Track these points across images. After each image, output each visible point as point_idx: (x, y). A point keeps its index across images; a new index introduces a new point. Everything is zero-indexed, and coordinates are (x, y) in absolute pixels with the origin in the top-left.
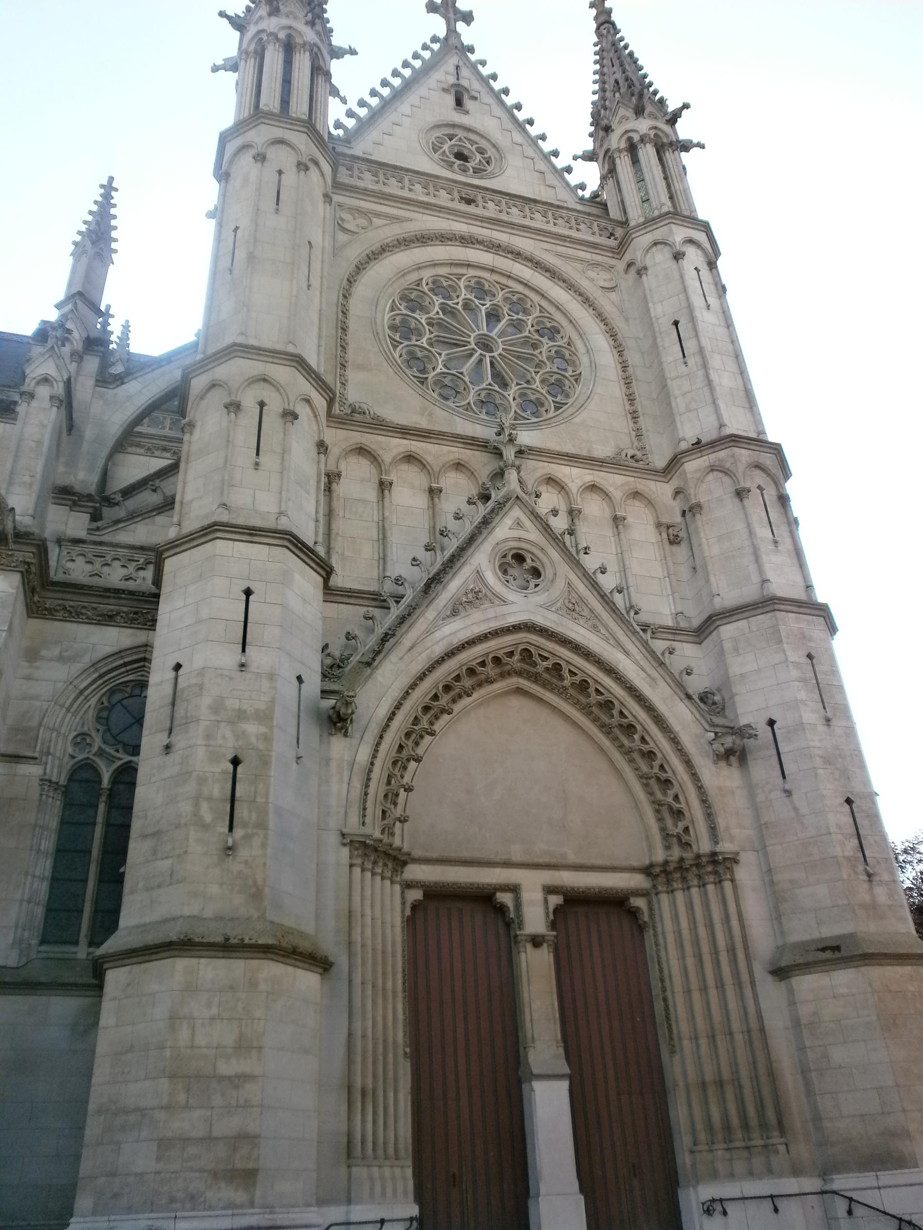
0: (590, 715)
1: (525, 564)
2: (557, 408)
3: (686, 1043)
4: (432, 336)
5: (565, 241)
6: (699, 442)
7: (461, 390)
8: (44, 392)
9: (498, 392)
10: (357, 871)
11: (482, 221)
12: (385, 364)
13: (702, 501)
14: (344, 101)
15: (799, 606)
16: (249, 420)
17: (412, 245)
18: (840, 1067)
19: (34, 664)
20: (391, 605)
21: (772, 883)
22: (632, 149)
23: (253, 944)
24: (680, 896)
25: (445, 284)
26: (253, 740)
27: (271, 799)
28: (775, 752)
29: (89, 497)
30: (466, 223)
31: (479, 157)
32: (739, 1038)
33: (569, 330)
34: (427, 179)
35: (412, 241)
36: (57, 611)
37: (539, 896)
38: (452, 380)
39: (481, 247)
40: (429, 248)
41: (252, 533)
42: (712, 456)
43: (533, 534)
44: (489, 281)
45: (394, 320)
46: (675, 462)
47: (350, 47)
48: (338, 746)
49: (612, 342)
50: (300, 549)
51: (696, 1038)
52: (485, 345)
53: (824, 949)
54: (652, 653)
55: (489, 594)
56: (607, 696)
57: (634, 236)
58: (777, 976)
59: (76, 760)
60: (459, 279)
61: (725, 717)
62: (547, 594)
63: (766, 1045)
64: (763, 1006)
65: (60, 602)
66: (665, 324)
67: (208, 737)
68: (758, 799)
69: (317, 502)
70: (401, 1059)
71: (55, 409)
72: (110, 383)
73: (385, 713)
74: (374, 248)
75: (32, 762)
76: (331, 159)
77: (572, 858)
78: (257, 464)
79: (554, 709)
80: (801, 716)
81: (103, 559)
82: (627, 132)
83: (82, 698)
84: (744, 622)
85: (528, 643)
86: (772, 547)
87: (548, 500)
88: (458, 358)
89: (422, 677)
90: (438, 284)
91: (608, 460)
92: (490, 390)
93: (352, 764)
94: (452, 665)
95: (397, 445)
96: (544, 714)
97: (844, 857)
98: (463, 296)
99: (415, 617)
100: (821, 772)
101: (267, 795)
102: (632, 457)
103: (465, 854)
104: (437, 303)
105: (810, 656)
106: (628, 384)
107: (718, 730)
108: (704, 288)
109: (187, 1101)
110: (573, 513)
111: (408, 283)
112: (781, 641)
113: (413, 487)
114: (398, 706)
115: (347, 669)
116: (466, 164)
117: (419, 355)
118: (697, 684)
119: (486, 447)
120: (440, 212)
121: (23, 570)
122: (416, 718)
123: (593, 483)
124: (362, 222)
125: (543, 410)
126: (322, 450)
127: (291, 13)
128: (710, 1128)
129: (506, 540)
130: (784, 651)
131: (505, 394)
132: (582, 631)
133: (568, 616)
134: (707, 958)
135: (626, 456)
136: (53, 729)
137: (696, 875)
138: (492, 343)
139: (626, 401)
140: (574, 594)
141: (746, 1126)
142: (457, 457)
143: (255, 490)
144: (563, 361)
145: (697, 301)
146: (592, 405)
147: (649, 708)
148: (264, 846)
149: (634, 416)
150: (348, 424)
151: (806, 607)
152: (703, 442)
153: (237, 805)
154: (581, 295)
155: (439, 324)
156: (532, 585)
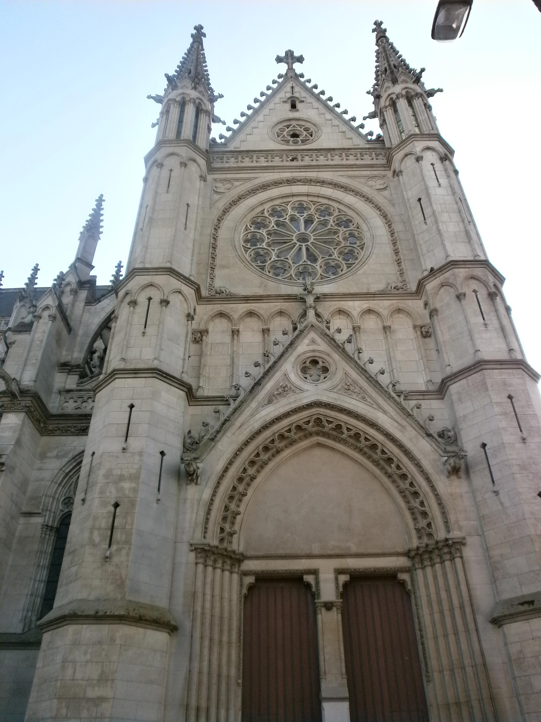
1: (318, 366)
2: (348, 267)
3: (436, 676)
4: (269, 240)
5: (353, 168)
6: (432, 269)
7: (287, 268)
8: (46, 314)
9: (310, 265)
10: (201, 567)
11: (299, 169)
12: (239, 262)
14: (224, 123)
15: (501, 364)
16: (141, 310)
17: (258, 192)
19: (44, 461)
20: (231, 403)
21: (490, 558)
22: (393, 104)
23: (112, 615)
24: (429, 570)
25: (279, 209)
26: (127, 492)
27: (134, 526)
28: (486, 465)
29: (78, 366)
30: (332, 171)
31: (305, 133)
32: (469, 670)
33: (357, 219)
34: (280, 153)
36: (55, 430)
37: (332, 576)
38: (282, 264)
39: (301, 183)
40: (268, 191)
41: (136, 372)
43: (322, 346)
44: (306, 202)
45: (247, 236)
46: (421, 285)
47: (219, 94)
48: (192, 491)
50: (165, 377)
51: (441, 671)
52: (303, 239)
53: (522, 604)
54: (403, 409)
55: (292, 387)
56: (373, 441)
58: (496, 624)
59: (64, 512)
60: (287, 205)
61: (457, 446)
62: (331, 381)
63: (488, 677)
64: (485, 646)
65: (56, 425)
66: (414, 201)
67: (101, 492)
68: (478, 500)
69: (185, 348)
70: (233, 687)
71: (51, 322)
72: (93, 303)
74: (233, 199)
75: (38, 515)
76: (204, 156)
77: (354, 549)
78: (144, 333)
79: (343, 454)
80: (502, 439)
81: (82, 399)
82: (389, 95)
83: (68, 477)
84: (464, 381)
86: (483, 328)
87: (338, 322)
88: (286, 250)
89: (246, 443)
90: (275, 210)
91: (378, 293)
92: (305, 265)
93: (199, 501)
94: (268, 433)
95: (243, 307)
98: (289, 214)
99: (243, 408)
100: (518, 476)
101: (132, 524)
102: (395, 288)
103: (281, 552)
104: (273, 221)
105: (510, 397)
106: (394, 244)
107: (449, 454)
109: (67, 715)
110: (356, 329)
111: (256, 213)
112: (487, 389)
114: (231, 463)
115: (201, 444)
117: (262, 253)
118: (435, 427)
119: (296, 299)
120: (274, 169)
121: (25, 410)
122: (245, 469)
123: (368, 308)
124: (228, 186)
125: (339, 270)
126: (189, 318)
127: (184, 86)
129: (305, 353)
130: (489, 396)
131: (314, 265)
132: (354, 402)
133: (345, 394)
134: (447, 613)
135: (391, 288)
136: (50, 497)
137: (438, 555)
138: (307, 236)
140: (350, 380)
142: (279, 307)
143: (142, 348)
144: (355, 238)
145: (432, 183)
146: (371, 261)
147: (401, 446)
148: (128, 555)
149: (399, 263)
150: (263, 299)
151: (506, 364)
152: (435, 268)
153: (114, 531)
154: (363, 197)
155: (275, 233)
156: (322, 377)
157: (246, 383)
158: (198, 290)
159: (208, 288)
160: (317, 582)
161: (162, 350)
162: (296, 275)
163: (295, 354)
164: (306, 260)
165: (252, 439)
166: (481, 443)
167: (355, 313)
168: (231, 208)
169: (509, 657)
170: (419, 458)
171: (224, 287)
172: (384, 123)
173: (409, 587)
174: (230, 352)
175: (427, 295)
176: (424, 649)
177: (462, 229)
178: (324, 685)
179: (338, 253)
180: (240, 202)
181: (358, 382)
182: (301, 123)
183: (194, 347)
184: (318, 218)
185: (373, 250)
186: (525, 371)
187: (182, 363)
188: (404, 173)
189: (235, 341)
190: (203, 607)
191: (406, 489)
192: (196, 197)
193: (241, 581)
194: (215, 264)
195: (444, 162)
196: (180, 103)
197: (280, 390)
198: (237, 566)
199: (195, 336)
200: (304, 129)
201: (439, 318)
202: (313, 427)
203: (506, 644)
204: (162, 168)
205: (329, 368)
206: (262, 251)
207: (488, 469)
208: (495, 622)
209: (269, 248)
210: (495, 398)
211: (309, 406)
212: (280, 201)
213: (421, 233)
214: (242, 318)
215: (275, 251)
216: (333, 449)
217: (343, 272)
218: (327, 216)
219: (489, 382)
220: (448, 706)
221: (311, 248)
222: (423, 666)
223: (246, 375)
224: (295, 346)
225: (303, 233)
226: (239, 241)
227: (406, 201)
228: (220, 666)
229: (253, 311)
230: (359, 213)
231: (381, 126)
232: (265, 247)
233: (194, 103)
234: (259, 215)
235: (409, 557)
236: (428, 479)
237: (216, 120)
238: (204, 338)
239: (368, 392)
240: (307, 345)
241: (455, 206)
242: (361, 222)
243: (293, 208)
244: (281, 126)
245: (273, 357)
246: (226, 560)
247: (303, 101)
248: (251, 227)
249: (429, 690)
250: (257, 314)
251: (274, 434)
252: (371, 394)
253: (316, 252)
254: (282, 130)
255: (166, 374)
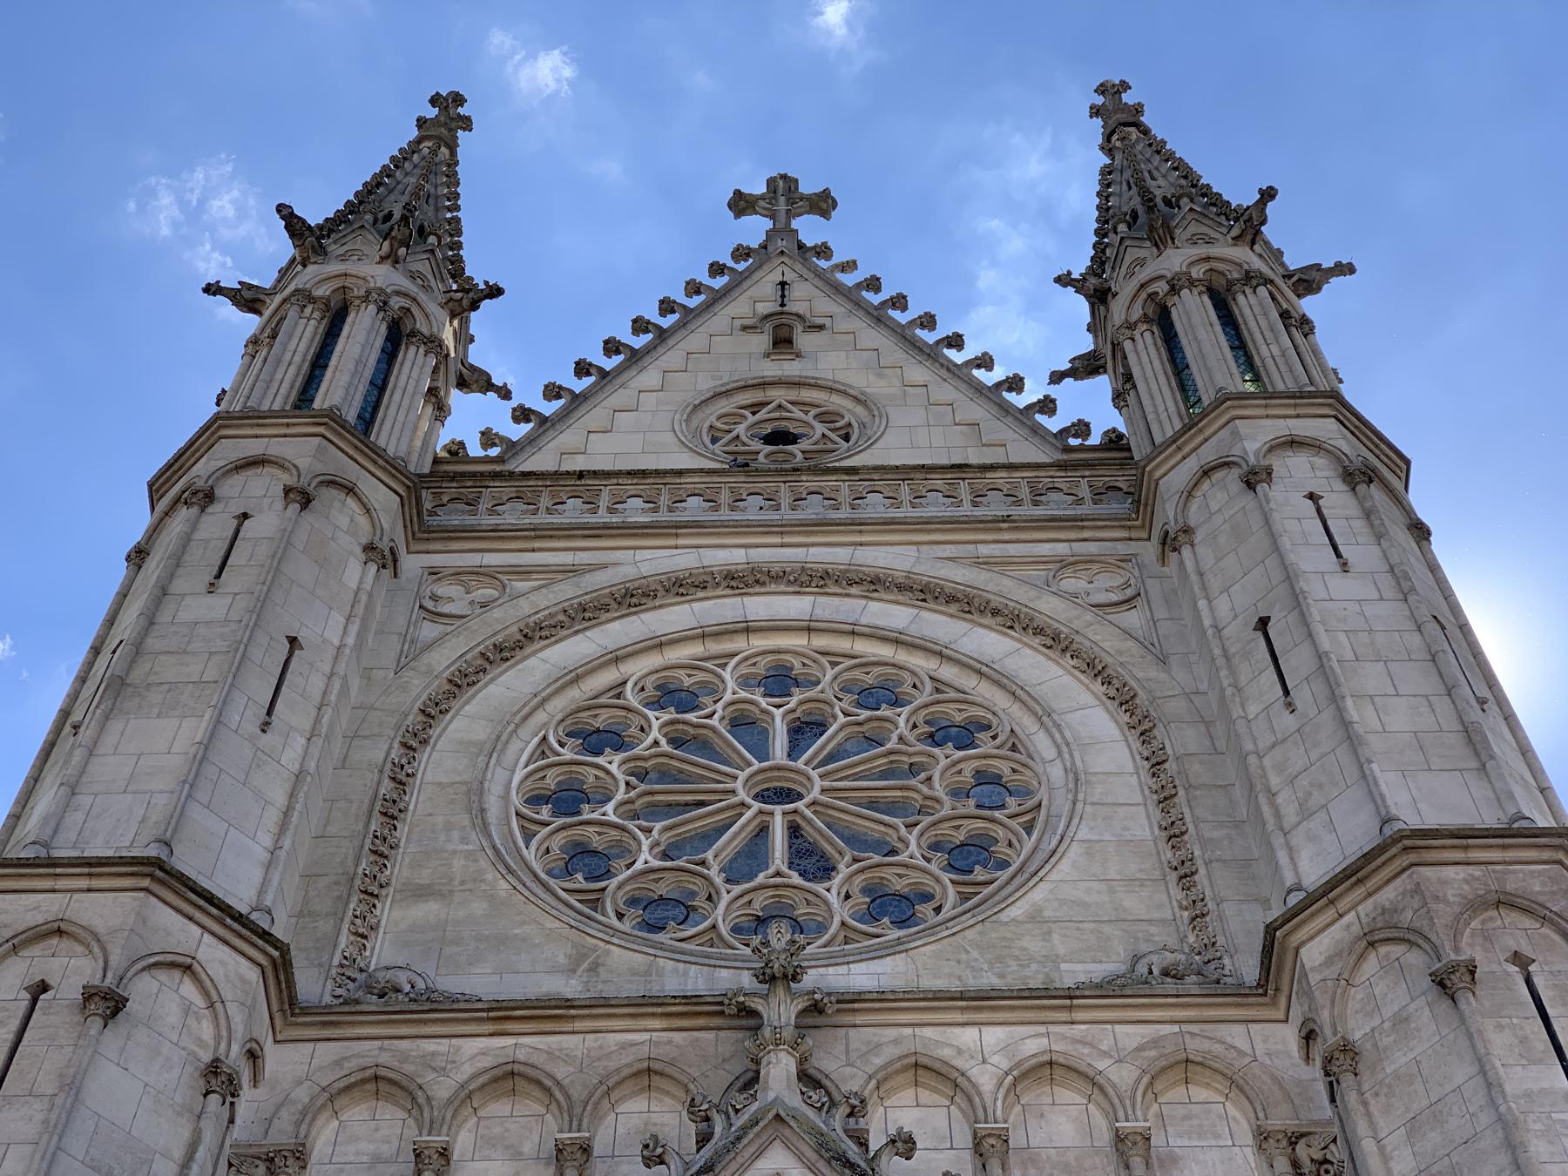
2: (965, 898)
4: (633, 794)
13: (1357, 1035)
17: (604, 616)
22: (1163, 321)
31: (820, 428)
35: (605, 608)
39: (782, 588)
40: (646, 616)
42: (1366, 908)
49: (1126, 718)
57: (1158, 474)
60: (723, 666)
66: (1240, 633)
92: (776, 886)
98: (728, 697)
102: (1165, 973)
104: (656, 724)
106: (1165, 800)
108: (1333, 530)
111: (590, 694)
113: (517, 1155)
116: (789, 447)
123: (1046, 1058)
139: (1162, 845)
145: (1312, 559)
146: (1064, 868)
149: (1186, 878)
154: (1039, 631)
158: (279, 968)
159: (334, 972)
164: (784, 869)
167: (985, 1078)
168: (485, 671)
171: (407, 968)
172: (1128, 386)
175: (1308, 993)
177: (1449, 721)
179: (924, 845)
180: (528, 650)
182: (807, 395)
184: (846, 714)
185: (1072, 828)
188: (1199, 537)
192: (338, 619)
194: (382, 878)
195: (1362, 488)
196: (327, 305)
200: (815, 417)
201: (1365, 1087)
204: (209, 510)
206: (600, 834)
209: (630, 825)
212: (696, 649)
213: (1273, 746)
215: (655, 833)
217: (941, 917)
218: (884, 706)
221: (809, 822)
225: (779, 768)
226: (505, 798)
227: (1210, 632)
229: (522, 1068)
230: (1019, 692)
231: (1119, 398)
232: (613, 818)
233: (383, 306)
234: (603, 700)
237: (475, 380)
241: (1415, 640)
242: (1027, 724)
243: (744, 682)
244: (725, 406)
247: (821, 327)
248: (562, 745)
253: (831, 844)
254: (734, 417)
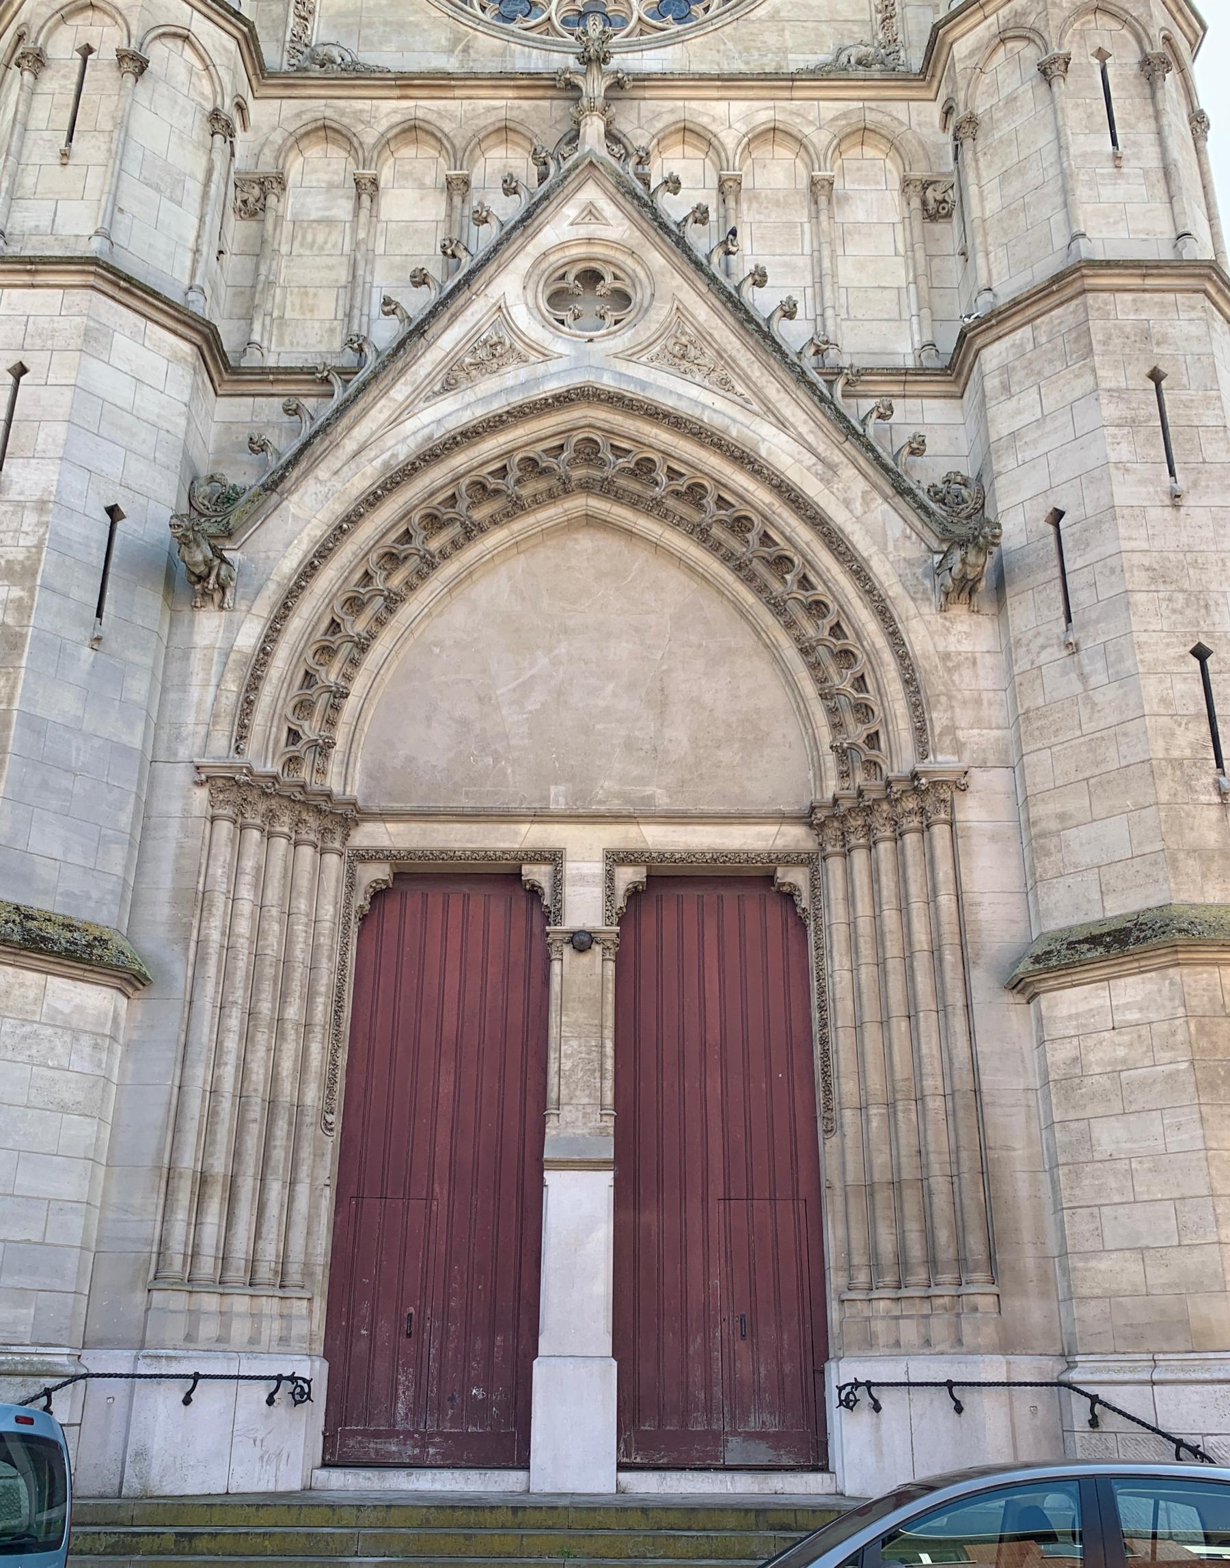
0: (717, 550)
1: (599, 287)
10: (224, 829)
18: (1112, 1159)
28: (1057, 572)
32: (935, 1104)
37: (597, 868)
50: (126, 290)
51: (863, 1108)
55: (519, 346)
58: (1021, 992)
64: (982, 1046)
73: (295, 564)
77: (663, 801)
85: (590, 426)
89: (373, 500)
94: (436, 475)
96: (640, 558)
97: (1171, 761)
100: (1139, 598)
102: (859, 62)
103: (464, 803)
105: (1156, 376)
110: (728, 188)
113: (422, 186)
123: (772, 125)
128: (874, 1265)
129: (562, 246)
130: (1094, 370)
132: (694, 392)
133: (671, 370)
134: (894, 966)
135: (849, 61)
141: (932, 1262)
142: (502, 114)
156: (609, 319)
157: (384, 332)
159: (287, 45)
160: (558, 882)
161: (121, 210)
162: (565, 22)
163: (534, 249)
165: (390, 490)
166: (1050, 510)
167: (729, 139)
169: (1045, 1074)
170: (865, 554)
173: (804, 902)
174: (347, 248)
176: (825, 1053)
178: (552, 1130)
181: (711, 335)
183: (237, 229)
186: (1215, 304)
187: (188, 263)
189: (364, 214)
190: (229, 931)
191: (820, 641)
193: (351, 874)
197: (482, 353)
198: (338, 836)
199: (246, 196)
201: (979, 148)
202: (571, 463)
203: (1041, 1042)
205: (630, 291)
207: (1059, 582)
208: (1020, 986)
210: (1110, 377)
211: (563, 400)
214: (388, 142)
216: (629, 534)
219: (1097, 328)
220: (870, 1189)
222: (820, 1095)
223: (386, 309)
224: (536, 223)
228: (274, 1079)
229: (421, 124)
235: (811, 825)
236: (883, 613)
238: (272, 200)
239: (738, 365)
240: (572, 224)
245: (469, 258)
246: (304, 816)
249: (829, 1148)
250: (433, 135)
251: (456, 479)
252: (749, 371)
255: (128, 279)
